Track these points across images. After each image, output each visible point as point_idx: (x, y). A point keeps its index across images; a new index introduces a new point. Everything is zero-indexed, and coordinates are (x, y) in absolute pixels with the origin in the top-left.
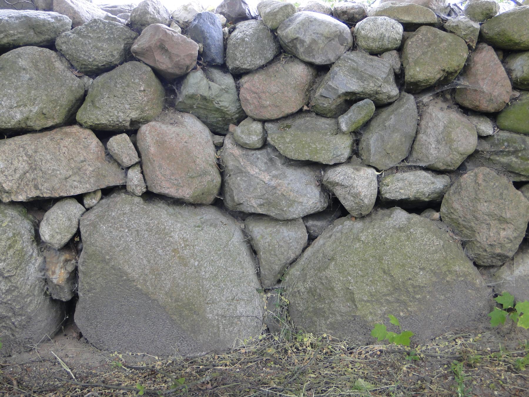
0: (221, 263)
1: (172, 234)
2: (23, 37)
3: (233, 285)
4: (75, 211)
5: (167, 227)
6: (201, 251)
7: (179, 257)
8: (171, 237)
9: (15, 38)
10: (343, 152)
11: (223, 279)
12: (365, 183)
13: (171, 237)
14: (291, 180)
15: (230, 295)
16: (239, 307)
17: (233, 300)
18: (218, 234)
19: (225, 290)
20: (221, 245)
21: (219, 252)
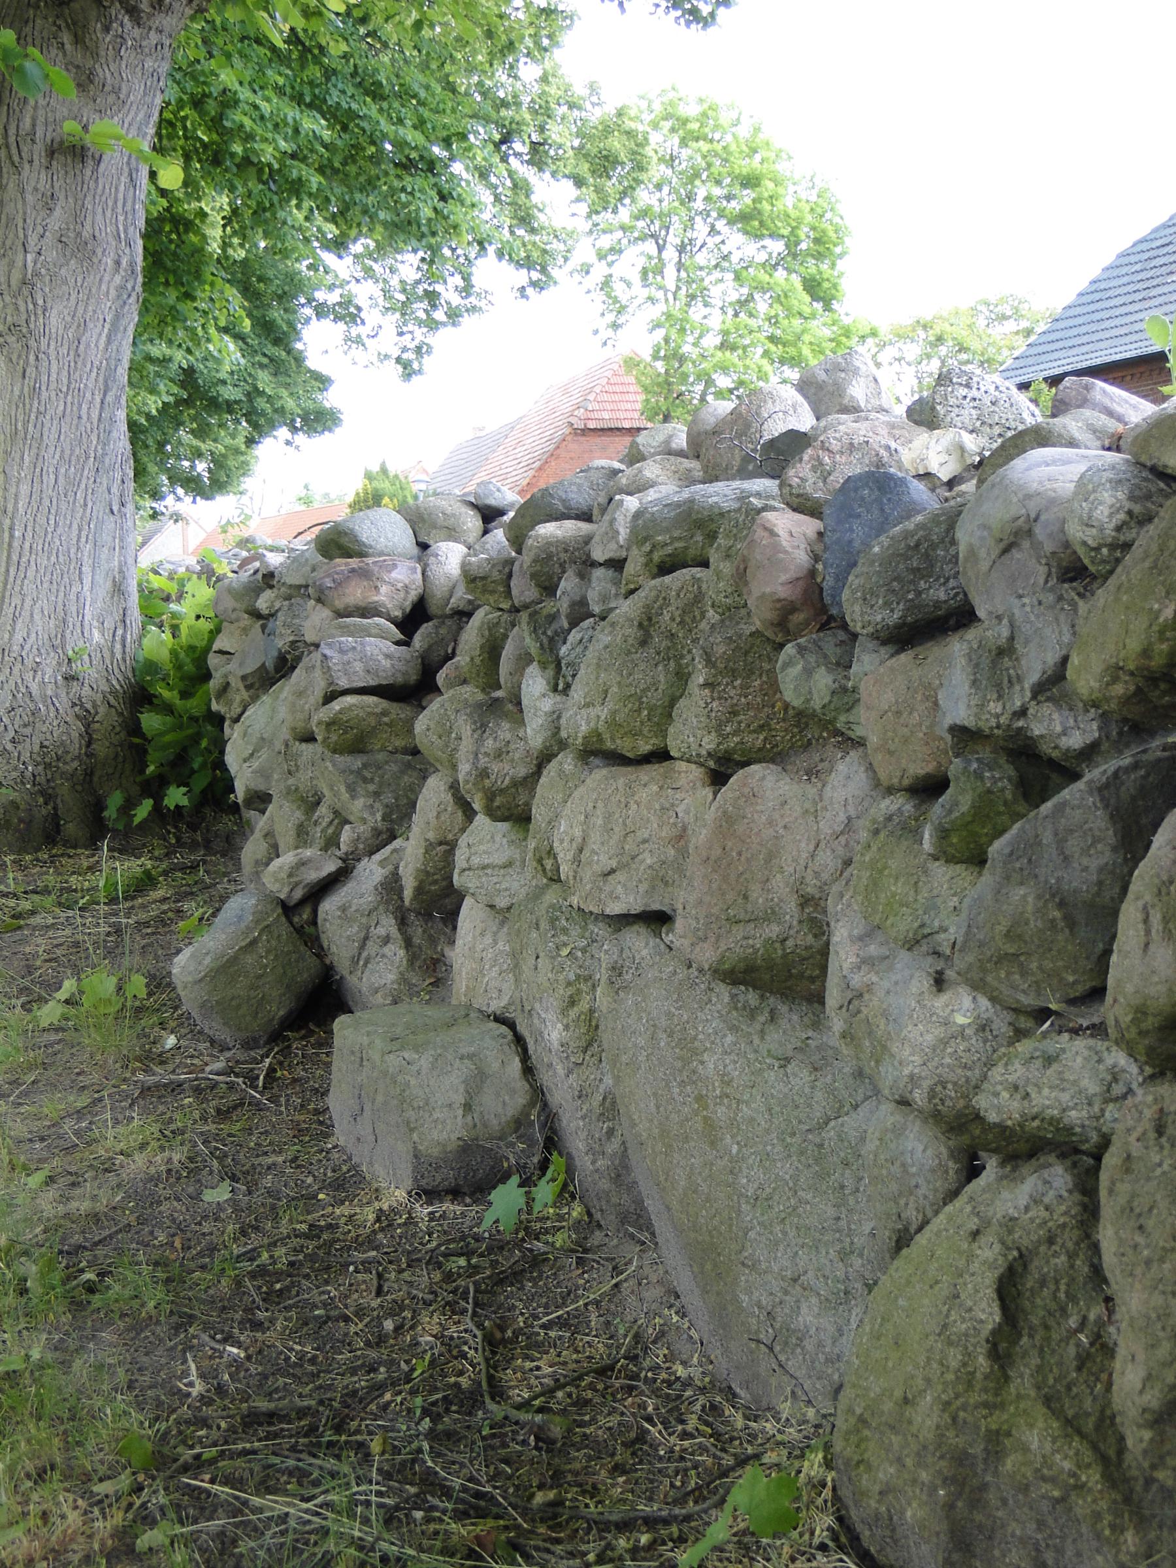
0: (784, 1169)
1: (706, 1057)
2: (686, 548)
3: (800, 1241)
4: (644, 952)
5: (701, 1036)
6: (752, 1120)
7: (705, 1118)
8: (702, 1063)
9: (669, 550)
10: (947, 922)
11: (783, 1215)
12: (929, 1037)
13: (702, 1063)
14: (896, 983)
15: (788, 1264)
16: (804, 1310)
17: (795, 1280)
18: (807, 1090)
19: (781, 1248)
20: (800, 1122)
21: (789, 1140)
